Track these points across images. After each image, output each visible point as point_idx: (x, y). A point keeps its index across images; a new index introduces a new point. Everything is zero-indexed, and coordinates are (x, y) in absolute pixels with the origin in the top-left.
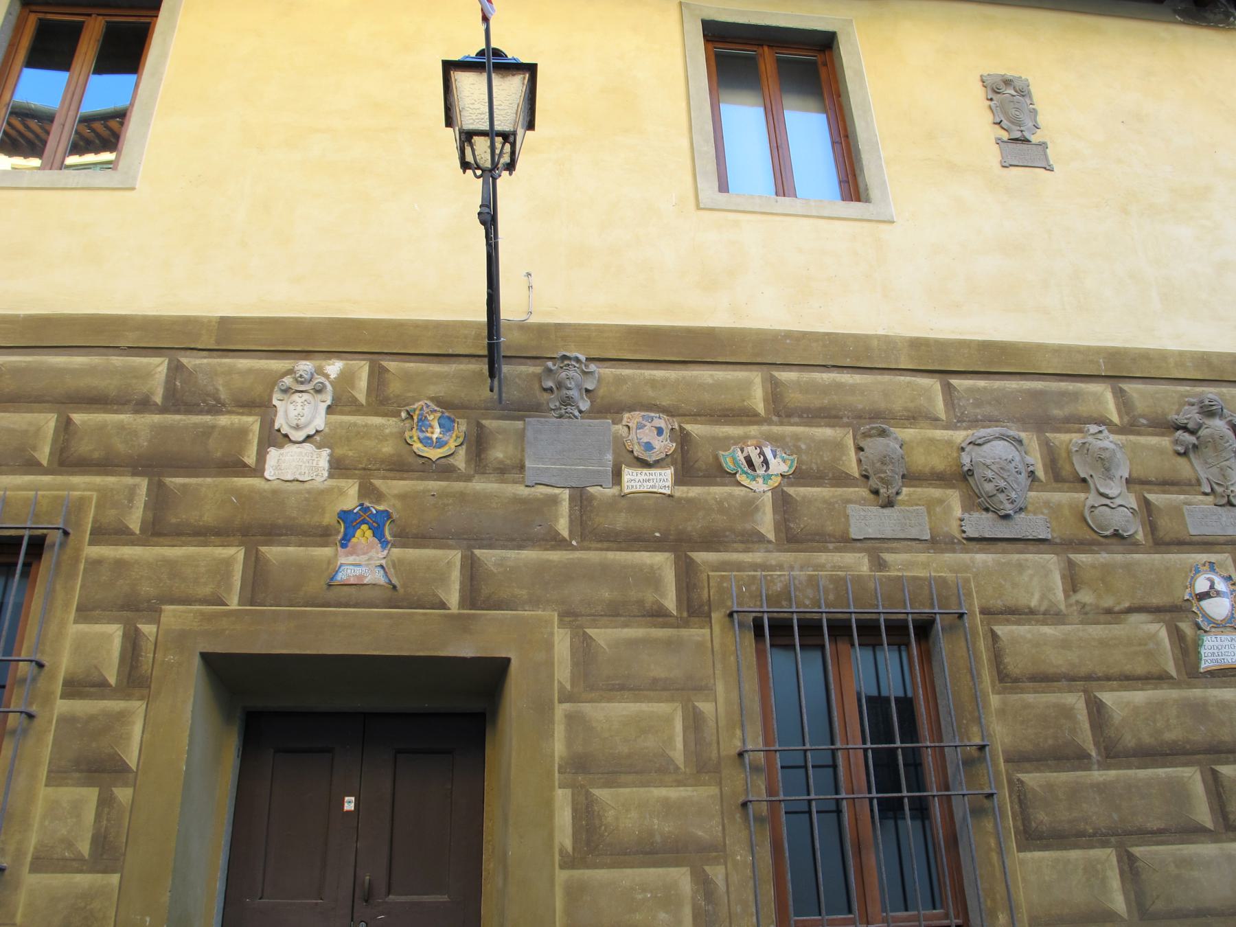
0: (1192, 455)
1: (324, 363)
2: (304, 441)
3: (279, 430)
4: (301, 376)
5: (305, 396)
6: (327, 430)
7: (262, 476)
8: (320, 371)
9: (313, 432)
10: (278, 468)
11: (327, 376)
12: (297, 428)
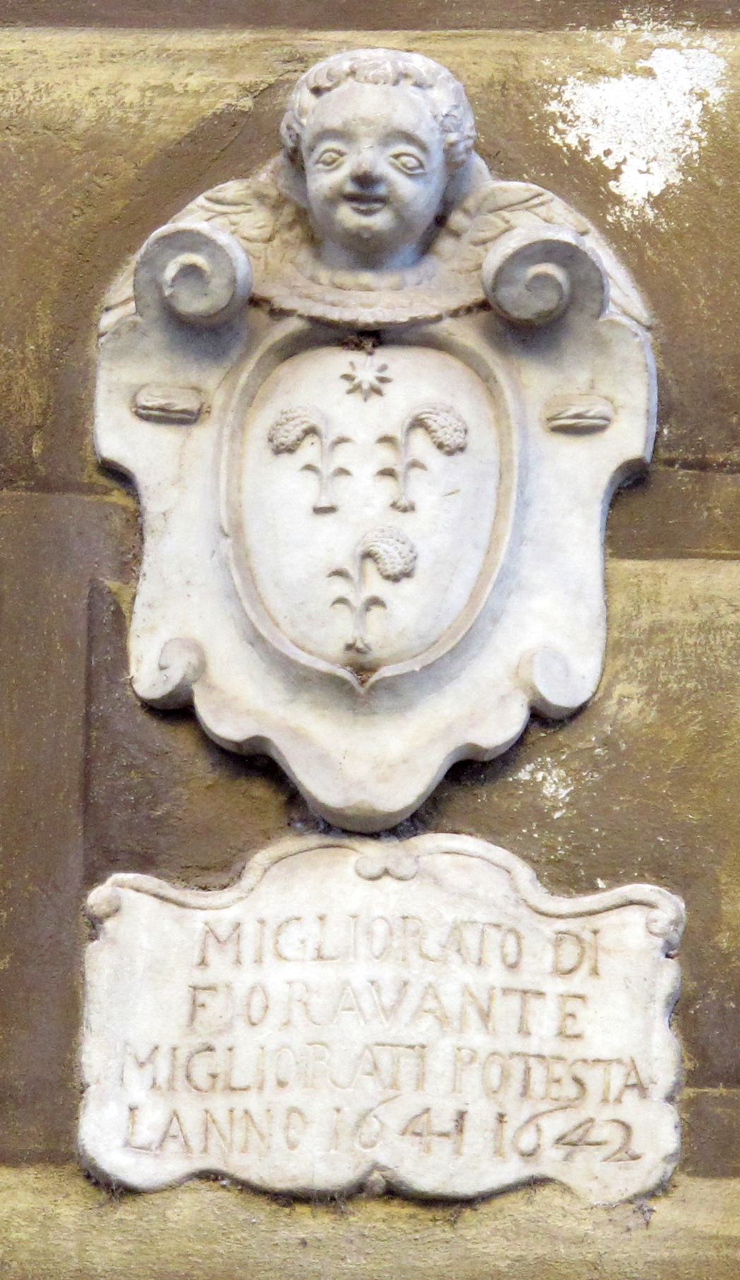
0: (297, 231)
1: (543, 53)
2: (424, 817)
3: (177, 710)
4: (366, 190)
5: (414, 380)
6: (630, 705)
7: (58, 1149)
8: (518, 137)
9: (498, 728)
10: (194, 1068)
11: (585, 182)
12: (359, 683)
